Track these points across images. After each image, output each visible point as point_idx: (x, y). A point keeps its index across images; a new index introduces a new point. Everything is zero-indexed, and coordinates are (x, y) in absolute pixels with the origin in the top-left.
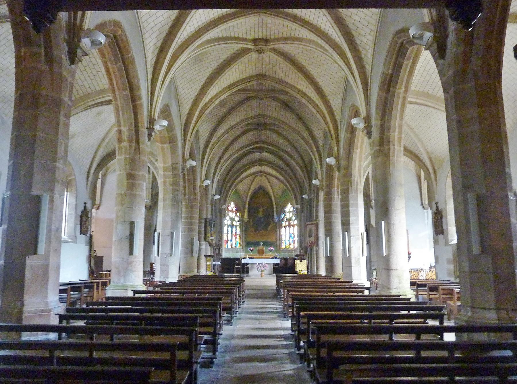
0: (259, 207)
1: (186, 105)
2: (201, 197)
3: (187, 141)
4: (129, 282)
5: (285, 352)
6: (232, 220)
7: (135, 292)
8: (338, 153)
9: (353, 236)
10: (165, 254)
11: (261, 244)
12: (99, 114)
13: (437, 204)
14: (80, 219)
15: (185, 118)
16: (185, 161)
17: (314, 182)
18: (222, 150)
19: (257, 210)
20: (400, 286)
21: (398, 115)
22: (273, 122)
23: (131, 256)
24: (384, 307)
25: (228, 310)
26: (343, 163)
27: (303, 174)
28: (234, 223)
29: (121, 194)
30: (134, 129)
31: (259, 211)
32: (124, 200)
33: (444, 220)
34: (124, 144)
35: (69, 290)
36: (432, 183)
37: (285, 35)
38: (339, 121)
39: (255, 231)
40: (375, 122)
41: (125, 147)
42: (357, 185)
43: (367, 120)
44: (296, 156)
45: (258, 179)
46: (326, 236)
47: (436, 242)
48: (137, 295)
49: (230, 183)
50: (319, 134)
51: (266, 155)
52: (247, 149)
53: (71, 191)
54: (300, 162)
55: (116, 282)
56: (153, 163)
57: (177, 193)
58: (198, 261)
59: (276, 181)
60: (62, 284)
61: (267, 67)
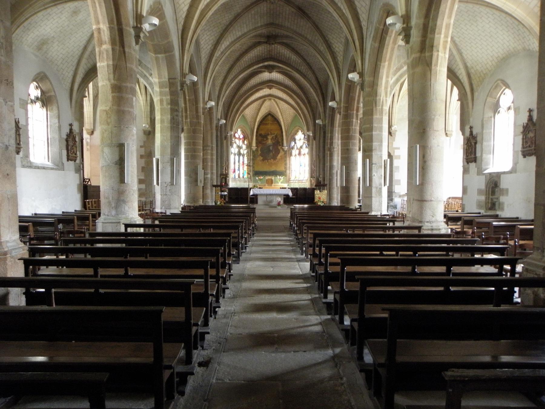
0: (268, 135)
1: (183, 5)
2: (205, 121)
3: (186, 51)
4: (124, 214)
5: (307, 298)
6: (239, 147)
7: (127, 226)
8: (362, 70)
9: (375, 164)
10: (165, 183)
12: (75, 12)
13: (471, 128)
14: (65, 143)
15: (182, 23)
16: (184, 75)
17: (330, 104)
18: (226, 68)
19: (265, 137)
20: (433, 219)
21: (447, 11)
22: (286, 33)
23: (122, 185)
24: (416, 244)
25: (236, 246)
26: (367, 79)
27: (318, 96)
28: (242, 151)
29: (105, 110)
30: (116, 28)
31: (267, 139)
32: (110, 117)
33: (478, 146)
34: (104, 47)
35: (57, 223)
36: (468, 104)
38: (364, 28)
39: (263, 160)
40: (416, 21)
41: (107, 51)
42: (382, 106)
43: (406, 18)
44: (310, 74)
45: (267, 104)
46: (342, 164)
47: (466, 171)
48: (129, 230)
49: (236, 107)
50: (339, 48)
51: (275, 75)
52: (255, 67)
53: (51, 110)
54: (315, 83)
55: (106, 214)
56: (148, 78)
57: (175, 113)
58: (203, 191)
59: (286, 106)
60: (22, 219)
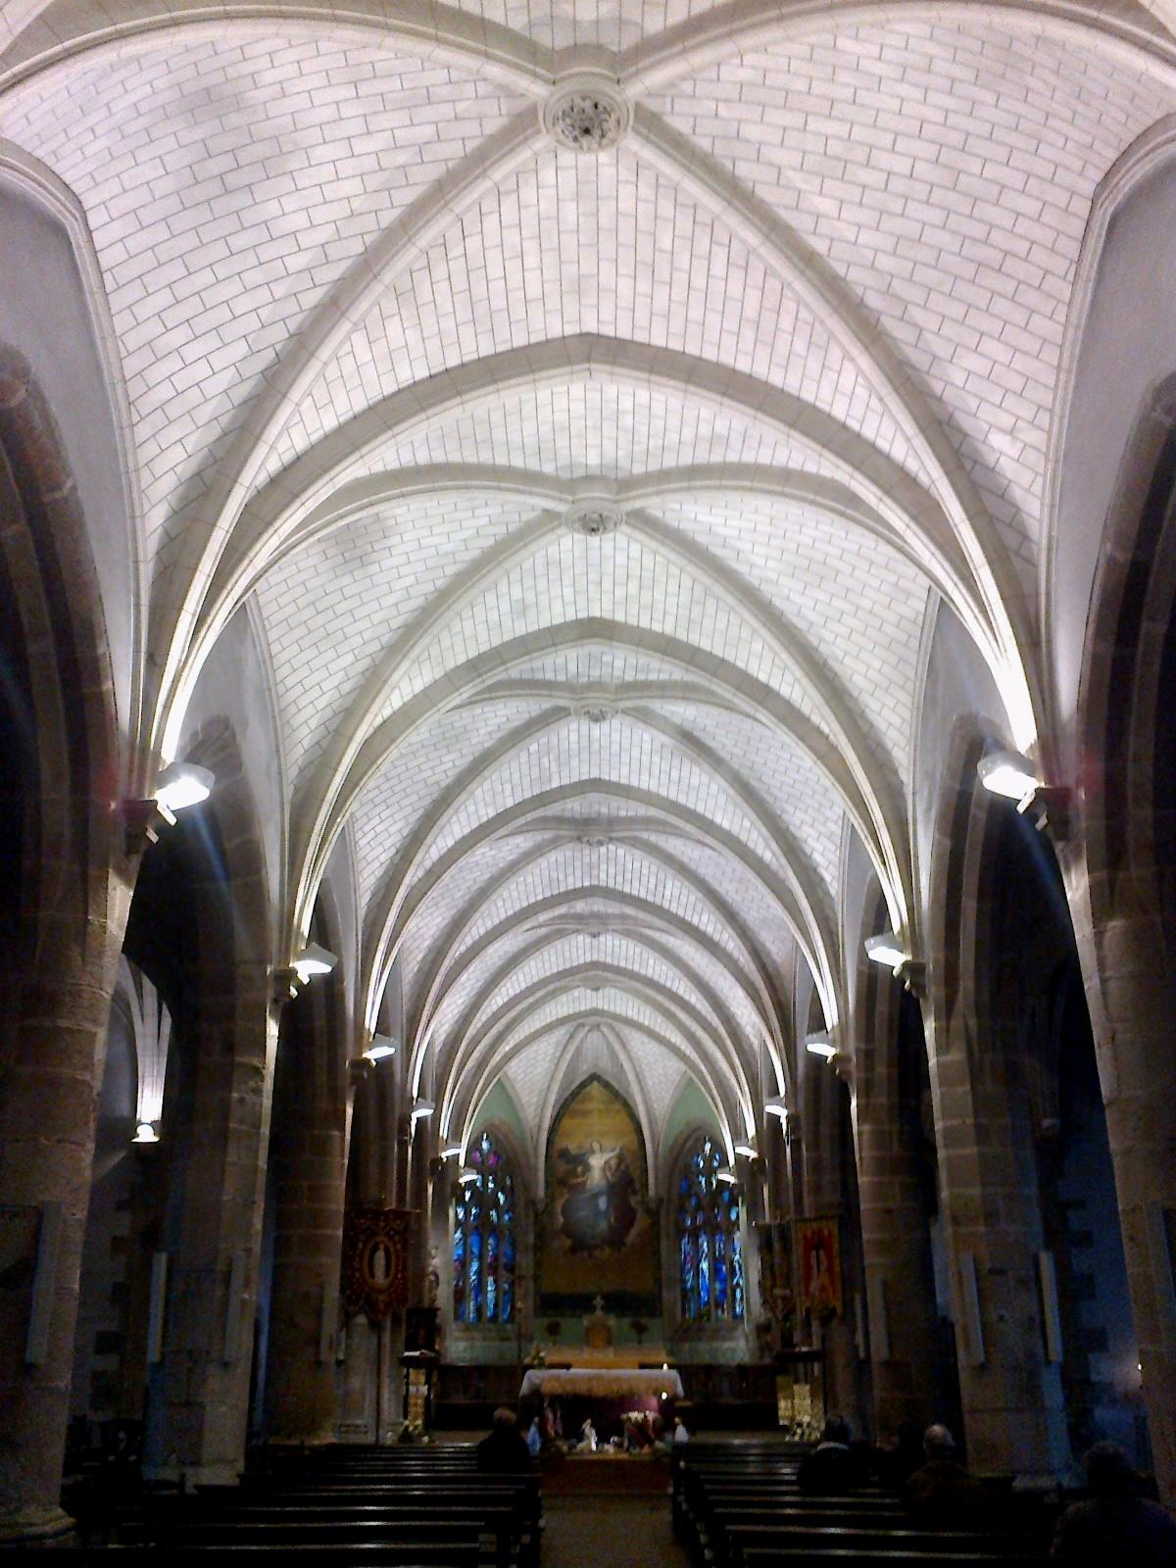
11: (599, 1301)
37: (686, 460)
59: (653, 1047)
61: (620, 592)
